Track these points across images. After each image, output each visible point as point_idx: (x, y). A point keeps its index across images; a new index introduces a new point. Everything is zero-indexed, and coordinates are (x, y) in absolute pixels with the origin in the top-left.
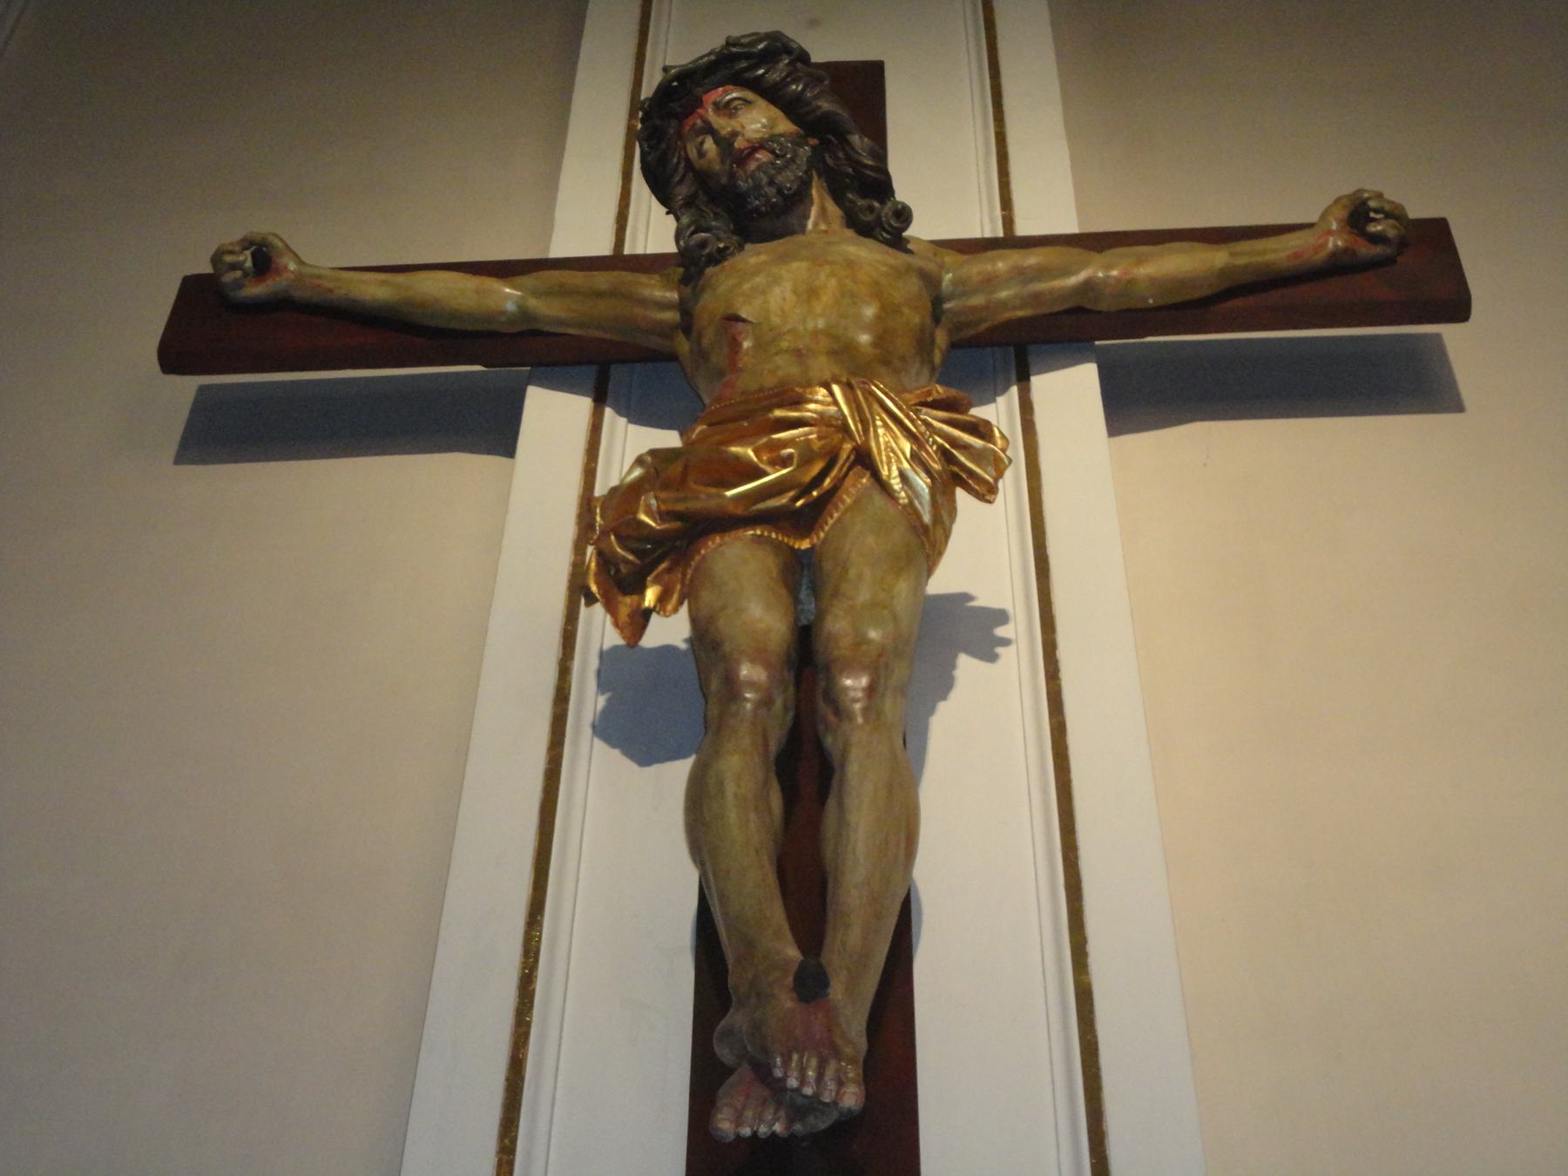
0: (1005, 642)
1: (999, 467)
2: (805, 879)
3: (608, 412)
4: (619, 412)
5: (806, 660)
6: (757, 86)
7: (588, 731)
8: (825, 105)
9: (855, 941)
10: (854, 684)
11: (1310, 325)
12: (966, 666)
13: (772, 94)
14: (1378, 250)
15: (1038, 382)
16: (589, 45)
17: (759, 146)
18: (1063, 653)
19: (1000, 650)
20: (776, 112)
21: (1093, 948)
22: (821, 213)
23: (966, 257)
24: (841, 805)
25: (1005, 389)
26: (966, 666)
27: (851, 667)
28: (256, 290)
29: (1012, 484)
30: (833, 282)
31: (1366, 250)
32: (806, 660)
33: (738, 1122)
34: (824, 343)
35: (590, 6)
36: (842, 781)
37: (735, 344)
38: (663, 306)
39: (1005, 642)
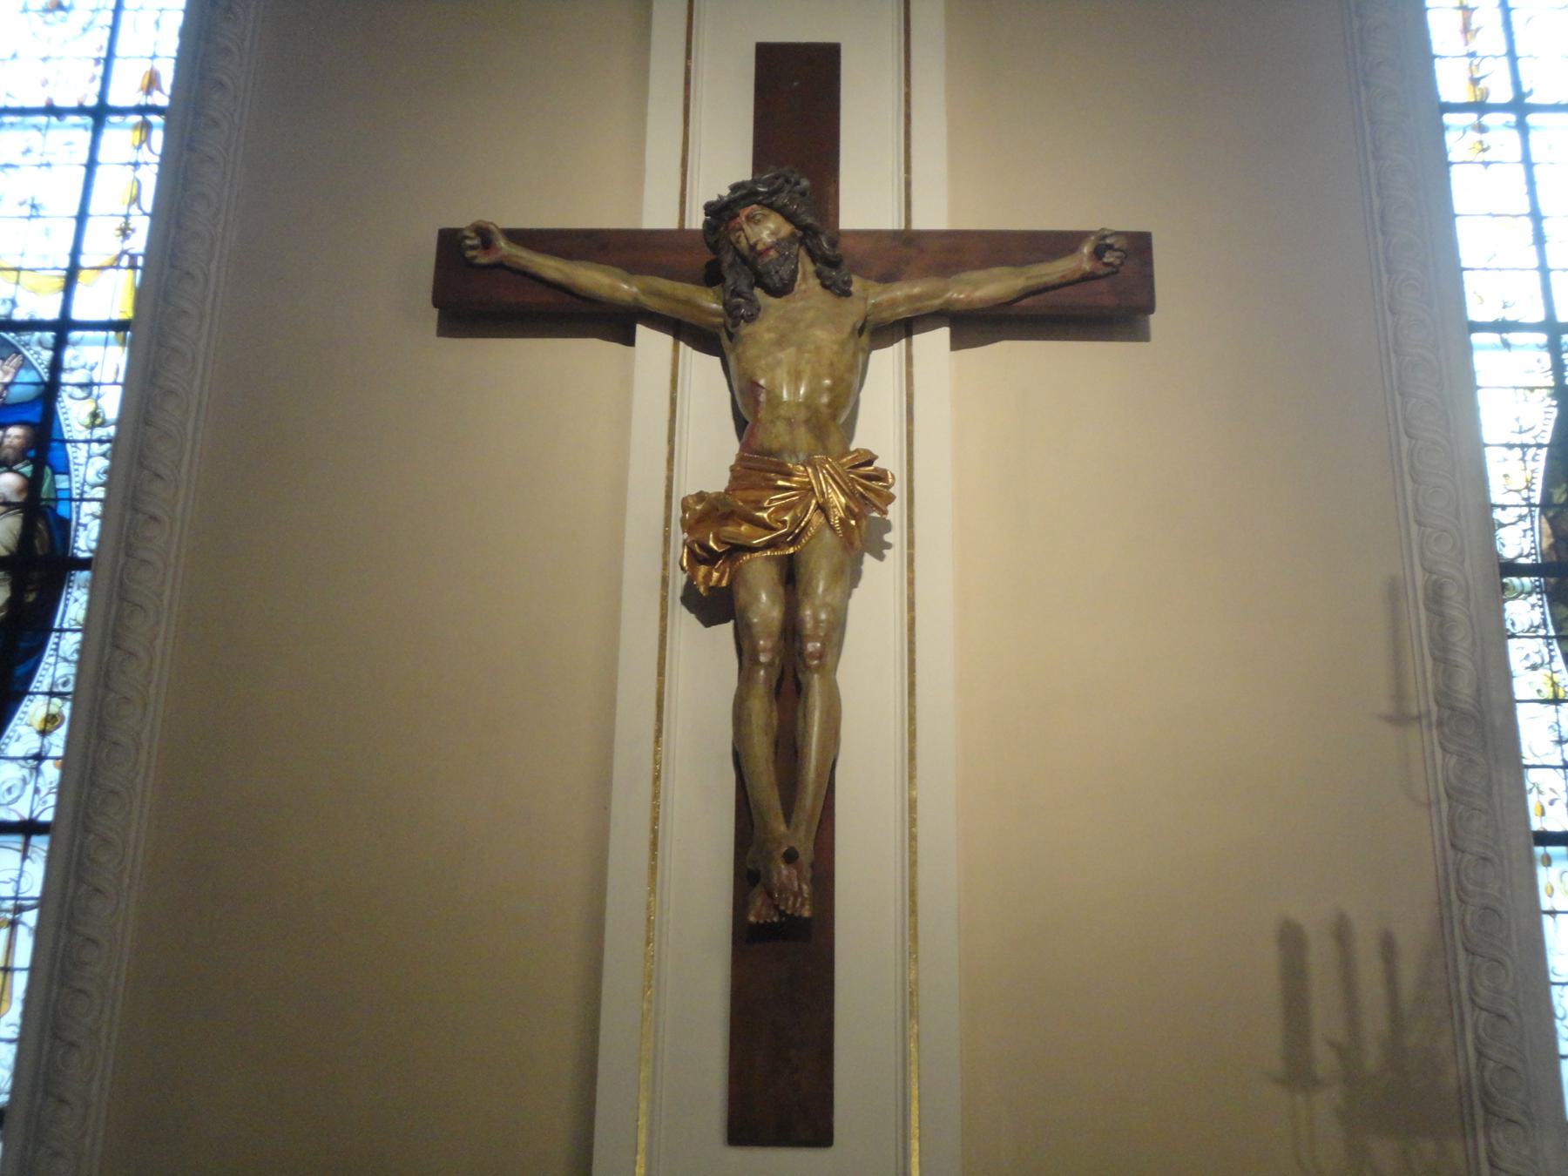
0: (889, 546)
1: (891, 498)
2: (788, 748)
3: (682, 344)
4: (688, 343)
5: (791, 631)
6: (770, 206)
8: (809, 220)
9: (809, 799)
10: (812, 647)
12: (868, 560)
13: (781, 211)
14: (1109, 270)
19: (886, 552)
21: (920, 773)
22: (808, 282)
24: (805, 707)
27: (815, 638)
28: (483, 260)
29: (894, 556)
31: (1102, 270)
32: (791, 631)
33: (758, 916)
34: (802, 415)
36: (806, 698)
37: (757, 402)
38: (714, 313)
39: (889, 546)
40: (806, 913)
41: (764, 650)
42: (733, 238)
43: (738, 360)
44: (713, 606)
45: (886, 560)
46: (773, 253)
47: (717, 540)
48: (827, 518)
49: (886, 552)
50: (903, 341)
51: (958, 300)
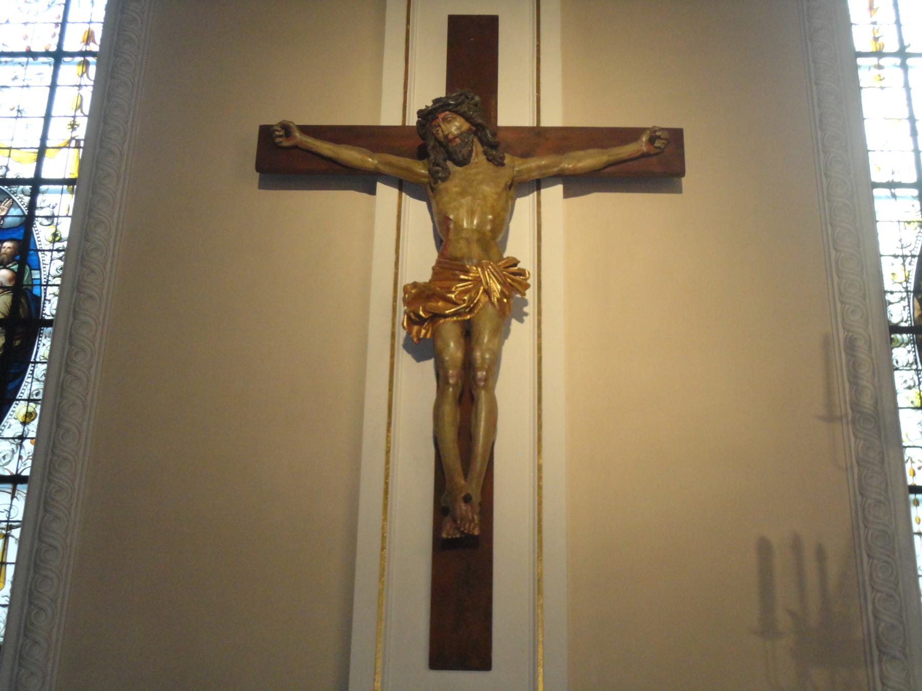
0: (526, 314)
2: (466, 435)
6: (456, 112)
7: (401, 347)
9: (478, 464)
11: (645, 163)
12: (514, 323)
13: (463, 115)
14: (658, 150)
15: (543, 191)
16: (389, 12)
17: (455, 137)
18: (544, 306)
19: (525, 318)
20: (462, 120)
22: (479, 157)
23: (524, 160)
25: (533, 192)
26: (514, 323)
27: (481, 369)
28: (286, 143)
30: (479, 208)
32: (468, 365)
33: (448, 534)
35: (388, 2)
37: (448, 229)
39: (526, 314)
42: (434, 132)
46: (458, 140)
49: (525, 318)
51: (568, 168)
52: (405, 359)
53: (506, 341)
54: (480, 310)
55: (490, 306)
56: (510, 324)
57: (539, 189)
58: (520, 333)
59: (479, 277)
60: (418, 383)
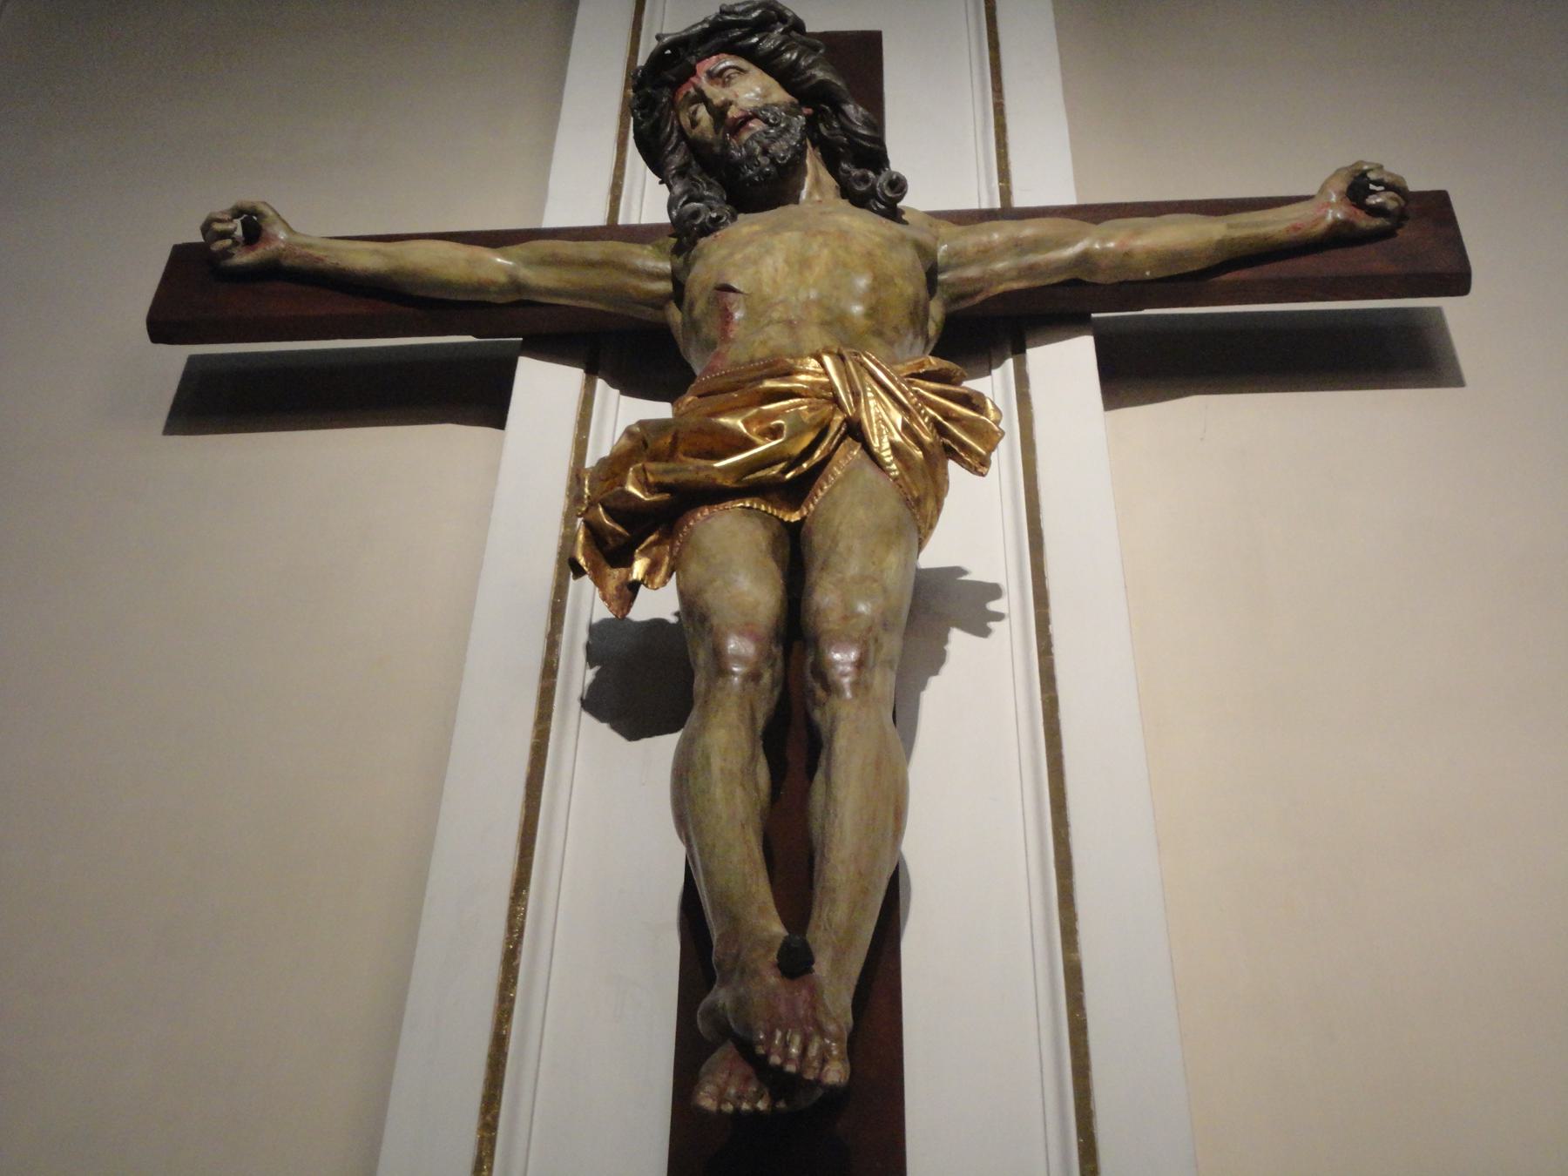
0: (999, 617)
4: (614, 382)
6: (751, 54)
9: (842, 918)
12: (959, 641)
13: (767, 63)
14: (1378, 222)
19: (992, 625)
20: (769, 81)
22: (816, 181)
26: (959, 641)
27: (843, 640)
28: (243, 258)
29: (1006, 457)
33: (721, 1098)
37: (726, 316)
39: (999, 617)
40: (835, 1073)
41: (739, 659)
42: (685, 121)
43: (757, 789)
44: (643, 683)
45: (992, 637)
46: (756, 125)
47: (645, 486)
48: (867, 447)
49: (992, 625)
50: (1010, 363)
51: (1104, 253)
52: (586, 742)
53: (933, 682)
54: (839, 481)
55: (870, 471)
56: (945, 467)
57: (1019, 350)
58: (971, 700)
59: (830, 386)
60: (622, 812)
